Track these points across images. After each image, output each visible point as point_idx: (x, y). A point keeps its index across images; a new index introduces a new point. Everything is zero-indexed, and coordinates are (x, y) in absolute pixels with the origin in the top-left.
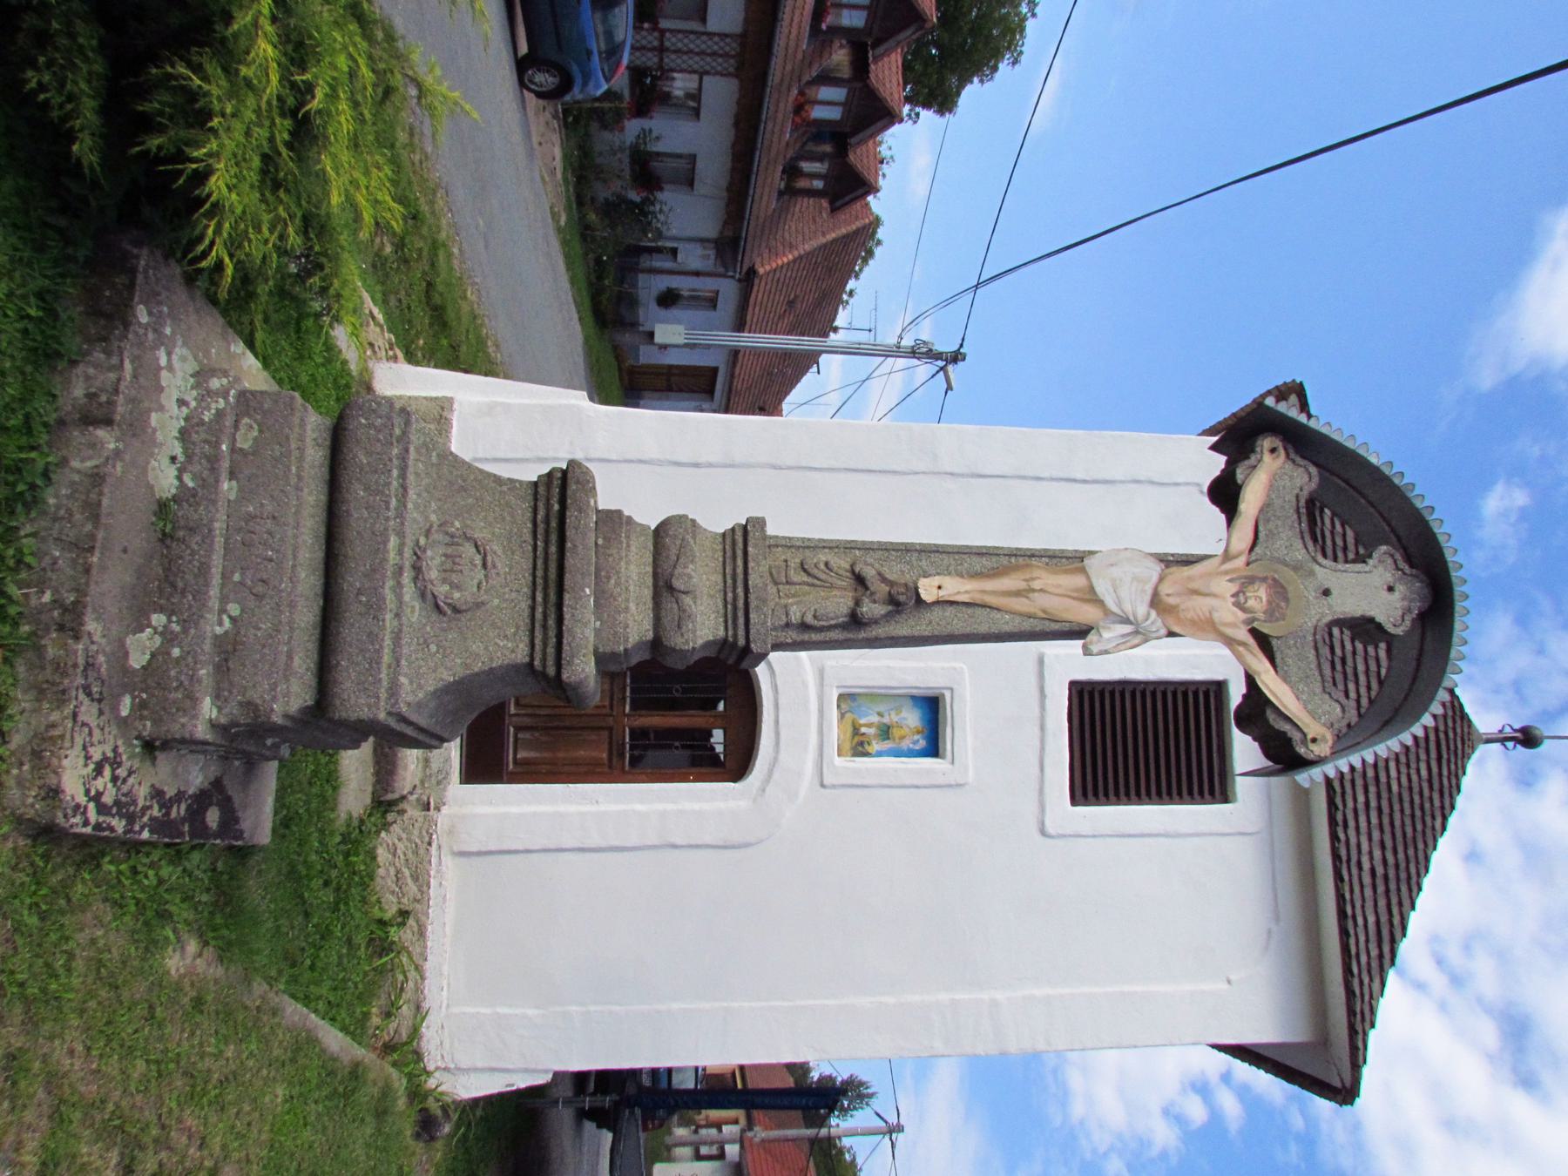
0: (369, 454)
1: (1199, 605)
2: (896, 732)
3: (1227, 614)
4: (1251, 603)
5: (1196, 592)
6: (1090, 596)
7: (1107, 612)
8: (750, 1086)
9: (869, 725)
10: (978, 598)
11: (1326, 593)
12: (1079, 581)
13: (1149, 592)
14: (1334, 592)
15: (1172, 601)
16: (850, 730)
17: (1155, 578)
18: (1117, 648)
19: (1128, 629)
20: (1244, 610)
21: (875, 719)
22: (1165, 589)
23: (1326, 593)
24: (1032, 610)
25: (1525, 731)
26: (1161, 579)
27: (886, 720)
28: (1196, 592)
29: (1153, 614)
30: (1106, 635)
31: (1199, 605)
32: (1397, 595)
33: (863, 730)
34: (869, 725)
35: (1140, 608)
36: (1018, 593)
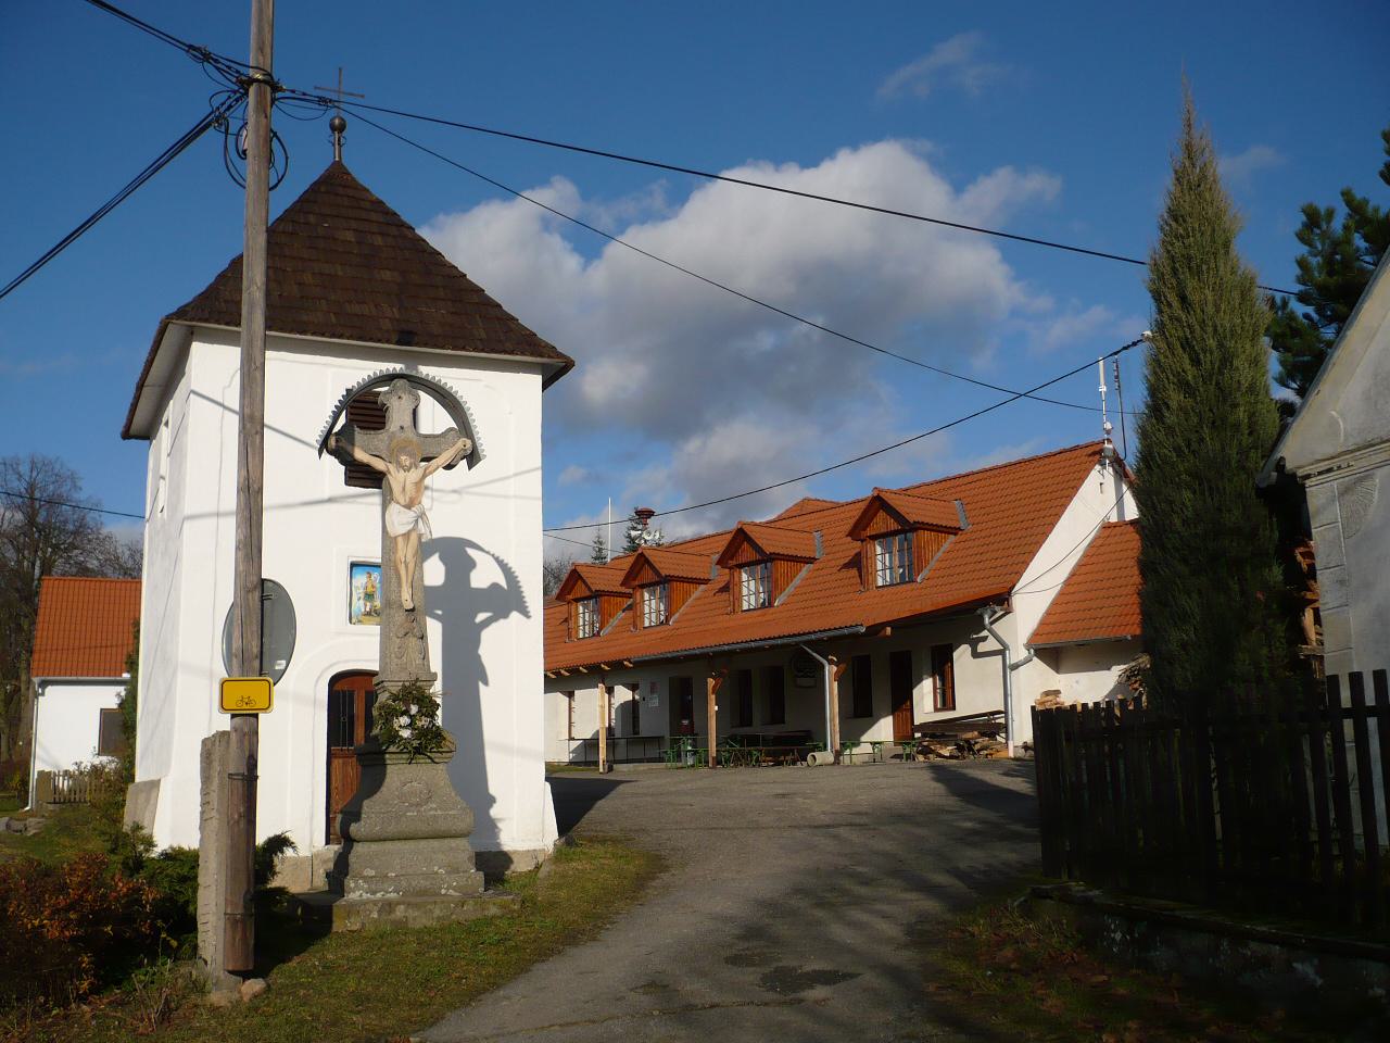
0: (376, 826)
1: (409, 487)
2: (370, 590)
3: (414, 475)
4: (408, 463)
5: (404, 489)
6: (407, 535)
7: (413, 529)
8: (1131, 628)
9: (366, 606)
10: (409, 584)
11: (402, 428)
12: (400, 540)
13: (403, 509)
14: (402, 424)
15: (408, 500)
16: (367, 617)
17: (398, 506)
18: (429, 527)
19: (420, 520)
20: (410, 468)
21: (362, 602)
22: (402, 502)
23: (402, 428)
24: (413, 561)
25: (333, 128)
26: (398, 503)
27: (362, 596)
28: (404, 489)
29: (413, 509)
30: (423, 531)
31: (409, 487)
32: (403, 395)
33: (368, 609)
34: (366, 606)
35: (411, 515)
36: (407, 567)
